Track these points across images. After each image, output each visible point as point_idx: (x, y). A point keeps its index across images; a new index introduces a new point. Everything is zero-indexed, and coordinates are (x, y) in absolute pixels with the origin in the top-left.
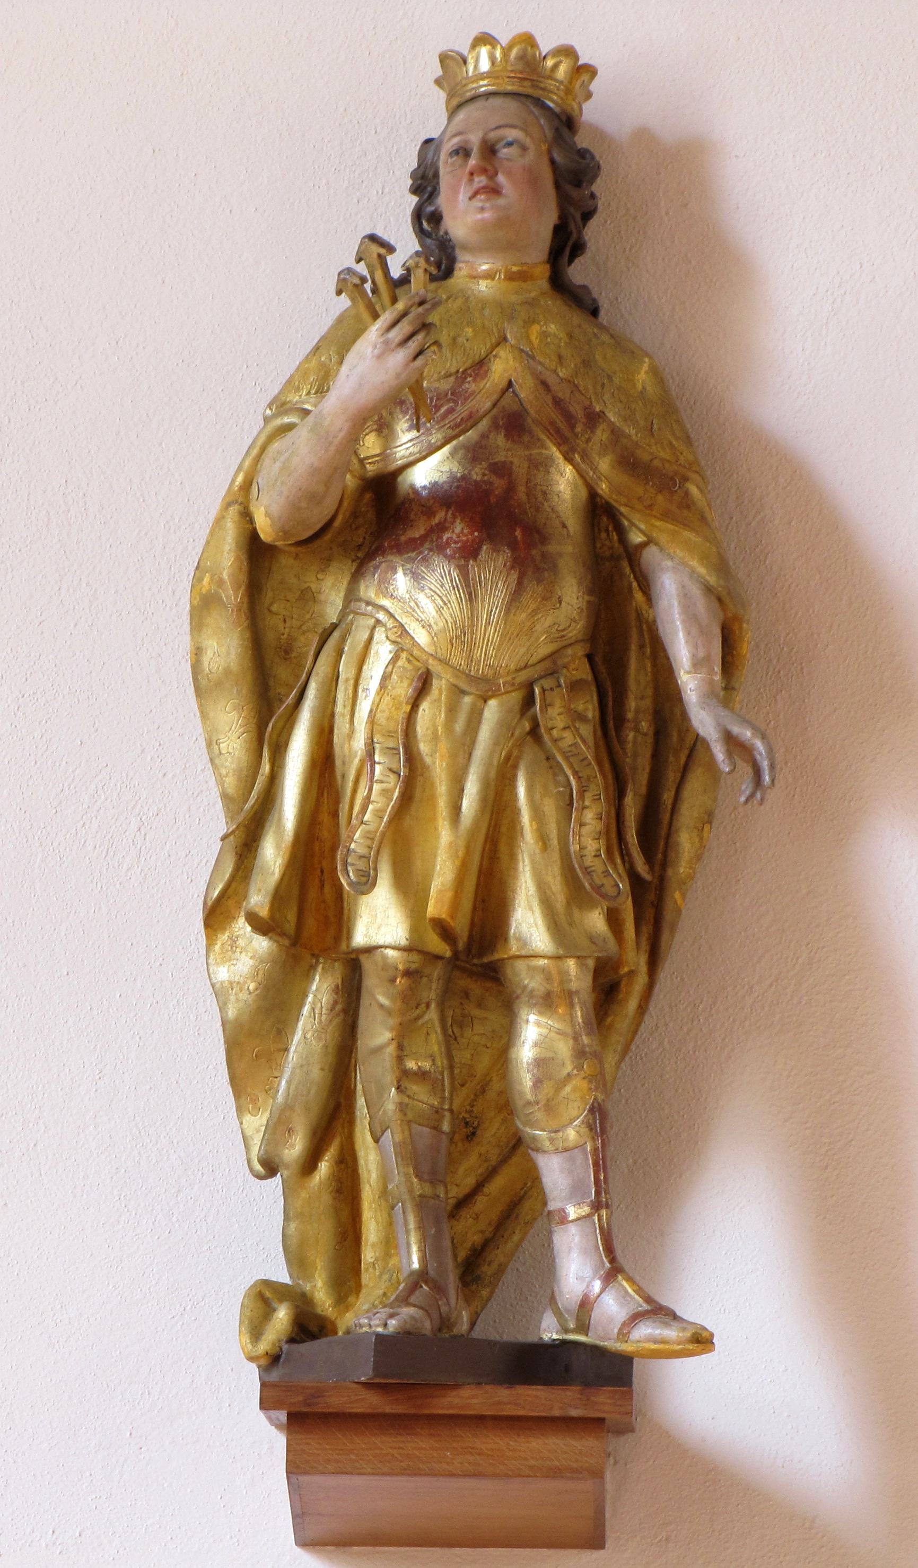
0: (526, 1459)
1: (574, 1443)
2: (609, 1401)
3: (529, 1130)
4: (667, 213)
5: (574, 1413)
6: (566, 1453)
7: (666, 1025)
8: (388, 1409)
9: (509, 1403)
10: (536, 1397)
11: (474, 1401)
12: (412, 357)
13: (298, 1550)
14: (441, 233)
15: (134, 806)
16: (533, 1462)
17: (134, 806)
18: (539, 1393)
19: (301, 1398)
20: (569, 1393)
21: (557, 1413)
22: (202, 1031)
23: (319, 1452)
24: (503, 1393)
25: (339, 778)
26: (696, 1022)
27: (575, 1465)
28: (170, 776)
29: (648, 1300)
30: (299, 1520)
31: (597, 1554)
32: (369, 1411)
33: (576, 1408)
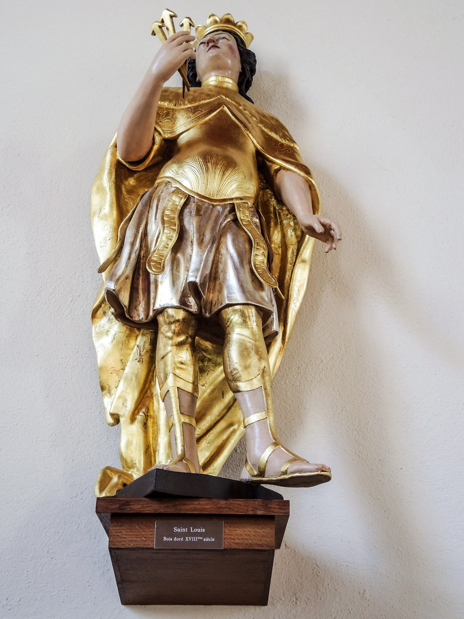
0: (234, 539)
1: (258, 531)
2: (277, 507)
3: (268, 163)
4: (279, 98)
5: (259, 513)
6: (254, 536)
7: (287, 375)
8: (162, 511)
9: (226, 508)
10: (239, 504)
11: (207, 507)
12: (183, 50)
13: (123, 607)
14: (197, 79)
15: (70, 293)
16: (237, 541)
17: (70, 293)
18: (241, 503)
19: (117, 506)
20: (256, 503)
21: (251, 513)
22: (93, 378)
23: (126, 536)
24: (223, 503)
25: (149, 242)
26: (300, 374)
27: (259, 543)
28: (85, 282)
29: (293, 455)
30: (121, 585)
31: (263, 608)
32: (153, 512)
33: (260, 510)
